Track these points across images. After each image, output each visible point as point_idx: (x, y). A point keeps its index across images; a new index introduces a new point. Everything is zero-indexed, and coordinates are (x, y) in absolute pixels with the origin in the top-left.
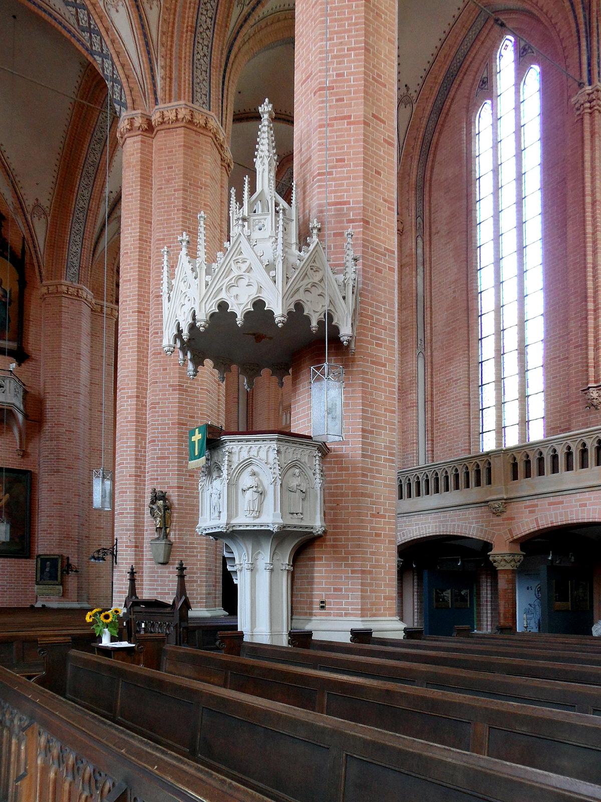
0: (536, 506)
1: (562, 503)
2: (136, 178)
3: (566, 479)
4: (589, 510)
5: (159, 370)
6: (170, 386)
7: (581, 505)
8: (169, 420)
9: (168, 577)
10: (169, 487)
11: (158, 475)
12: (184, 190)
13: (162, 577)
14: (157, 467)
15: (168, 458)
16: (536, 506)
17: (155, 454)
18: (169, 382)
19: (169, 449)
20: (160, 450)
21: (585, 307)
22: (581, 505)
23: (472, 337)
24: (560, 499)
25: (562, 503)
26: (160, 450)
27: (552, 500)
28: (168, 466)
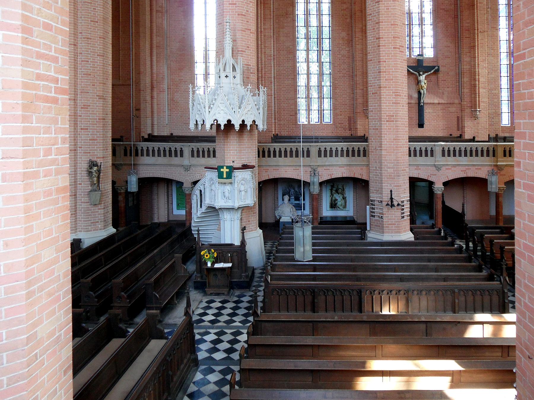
0: (268, 169)
1: (278, 170)
2: (384, 137)
3: (282, 161)
4: (288, 174)
5: (89, 85)
6: (97, 96)
7: (285, 171)
8: (97, 116)
9: (98, 212)
10: (97, 158)
11: (90, 150)
12: (380, 87)
13: (94, 212)
14: (90, 145)
15: (97, 140)
16: (268, 169)
17: (88, 137)
18: (96, 93)
19: (97, 135)
20: (91, 135)
21: (338, 111)
22: (285, 171)
23: (388, 196)
24: (278, 168)
25: (278, 170)
26: (91, 135)
27: (274, 168)
28: (97, 145)
